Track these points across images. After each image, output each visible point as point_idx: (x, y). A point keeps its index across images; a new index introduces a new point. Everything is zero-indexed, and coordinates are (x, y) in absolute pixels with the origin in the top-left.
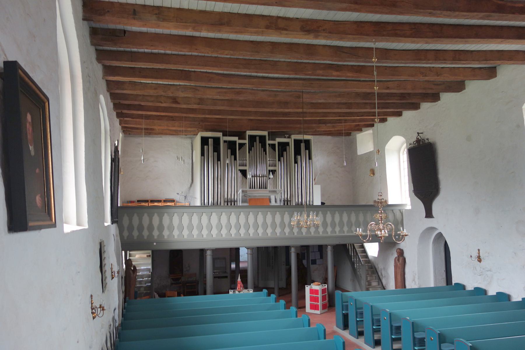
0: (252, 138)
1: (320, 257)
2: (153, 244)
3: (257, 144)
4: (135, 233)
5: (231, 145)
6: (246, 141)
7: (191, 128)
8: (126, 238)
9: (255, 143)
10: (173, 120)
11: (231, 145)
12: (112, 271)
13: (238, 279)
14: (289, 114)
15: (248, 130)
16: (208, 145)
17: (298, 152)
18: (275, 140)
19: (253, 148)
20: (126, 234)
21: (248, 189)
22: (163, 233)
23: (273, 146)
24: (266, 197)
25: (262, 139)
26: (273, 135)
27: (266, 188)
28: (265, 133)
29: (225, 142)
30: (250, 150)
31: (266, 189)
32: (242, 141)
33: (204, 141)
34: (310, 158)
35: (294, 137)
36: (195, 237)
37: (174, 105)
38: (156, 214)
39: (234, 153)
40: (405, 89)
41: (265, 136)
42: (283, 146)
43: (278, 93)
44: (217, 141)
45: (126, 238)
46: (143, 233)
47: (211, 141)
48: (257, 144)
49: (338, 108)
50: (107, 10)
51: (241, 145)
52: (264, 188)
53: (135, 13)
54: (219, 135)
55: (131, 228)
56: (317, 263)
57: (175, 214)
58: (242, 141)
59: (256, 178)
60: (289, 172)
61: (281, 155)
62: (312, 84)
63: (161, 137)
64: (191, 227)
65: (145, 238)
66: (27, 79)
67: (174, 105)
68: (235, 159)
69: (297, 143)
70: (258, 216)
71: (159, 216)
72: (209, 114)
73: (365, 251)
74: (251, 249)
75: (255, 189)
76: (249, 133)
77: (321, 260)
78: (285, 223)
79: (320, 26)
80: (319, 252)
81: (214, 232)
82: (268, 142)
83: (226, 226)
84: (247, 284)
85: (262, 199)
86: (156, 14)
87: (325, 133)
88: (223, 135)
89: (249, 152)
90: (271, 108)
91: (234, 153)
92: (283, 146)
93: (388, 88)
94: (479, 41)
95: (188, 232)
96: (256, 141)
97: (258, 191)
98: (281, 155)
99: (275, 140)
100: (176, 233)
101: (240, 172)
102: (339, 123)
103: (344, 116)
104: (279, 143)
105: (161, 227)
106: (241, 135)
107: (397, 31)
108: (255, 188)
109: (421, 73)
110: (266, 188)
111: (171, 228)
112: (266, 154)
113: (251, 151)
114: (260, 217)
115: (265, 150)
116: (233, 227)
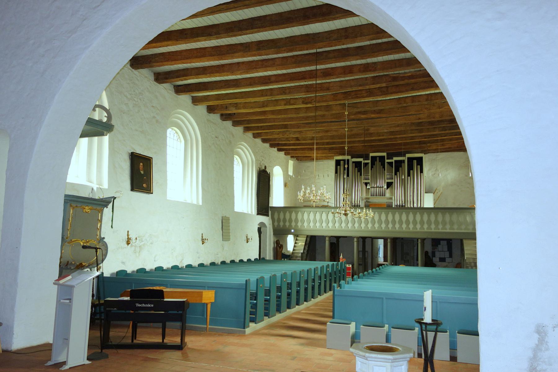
0: (374, 159)
1: (436, 253)
2: (292, 232)
3: (378, 163)
4: (282, 224)
5: (358, 165)
6: (369, 161)
7: (330, 154)
8: (276, 226)
9: (376, 162)
10: (311, 150)
11: (358, 165)
12: (247, 238)
13: (340, 256)
14: (384, 140)
15: (371, 153)
16: (340, 165)
17: (410, 168)
18: (393, 159)
19: (374, 166)
20: (276, 224)
21: (370, 196)
22: (292, 224)
23: (390, 164)
24: (384, 203)
25: (382, 158)
26: (390, 156)
27: (384, 196)
28: (384, 154)
29: (353, 162)
30: (372, 167)
31: (384, 197)
32: (366, 161)
33: (338, 163)
34: (422, 171)
35: (408, 155)
36: (311, 227)
37: (297, 142)
38: (293, 212)
39: (360, 171)
40: (434, 118)
41: (384, 157)
42: (399, 164)
43: (353, 129)
44: (348, 160)
45: (276, 226)
46: (286, 224)
47: (342, 163)
48: (378, 163)
49: (411, 133)
50: (215, 108)
51: (366, 164)
52: (381, 196)
53: (226, 108)
54: (349, 157)
55: (279, 220)
56: (446, 261)
57: (305, 212)
58: (366, 161)
59: (380, 189)
60: (403, 183)
61: (397, 170)
62: (362, 122)
63: (322, 161)
64: (315, 221)
65: (287, 227)
66: (148, 158)
67: (297, 142)
68: (361, 175)
69: (410, 160)
70: (329, 215)
71: (289, 213)
72: (326, 145)
73: (462, 250)
74: (356, 238)
75: (374, 196)
76: (372, 155)
77: (451, 259)
78: (349, 220)
79: (313, 100)
80: (448, 252)
81: (330, 225)
82: (387, 161)
83: (325, 221)
84: (477, 291)
85: (380, 204)
86: (235, 107)
87: (445, 150)
88: (352, 158)
89: (371, 169)
90: (360, 138)
91: (360, 171)
92: (399, 164)
93: (420, 118)
94: (401, 94)
95: (319, 225)
96: (376, 161)
97: (374, 198)
98: (397, 170)
99: (393, 159)
100: (306, 224)
101: (365, 184)
102: (436, 142)
103: (429, 138)
104: (395, 161)
105: (296, 221)
106: (366, 157)
107: (357, 95)
108: (382, 196)
109: (425, 109)
110: (384, 196)
111: (303, 221)
112: (385, 170)
113: (372, 169)
114: (324, 215)
115: (384, 167)
116: (343, 222)
